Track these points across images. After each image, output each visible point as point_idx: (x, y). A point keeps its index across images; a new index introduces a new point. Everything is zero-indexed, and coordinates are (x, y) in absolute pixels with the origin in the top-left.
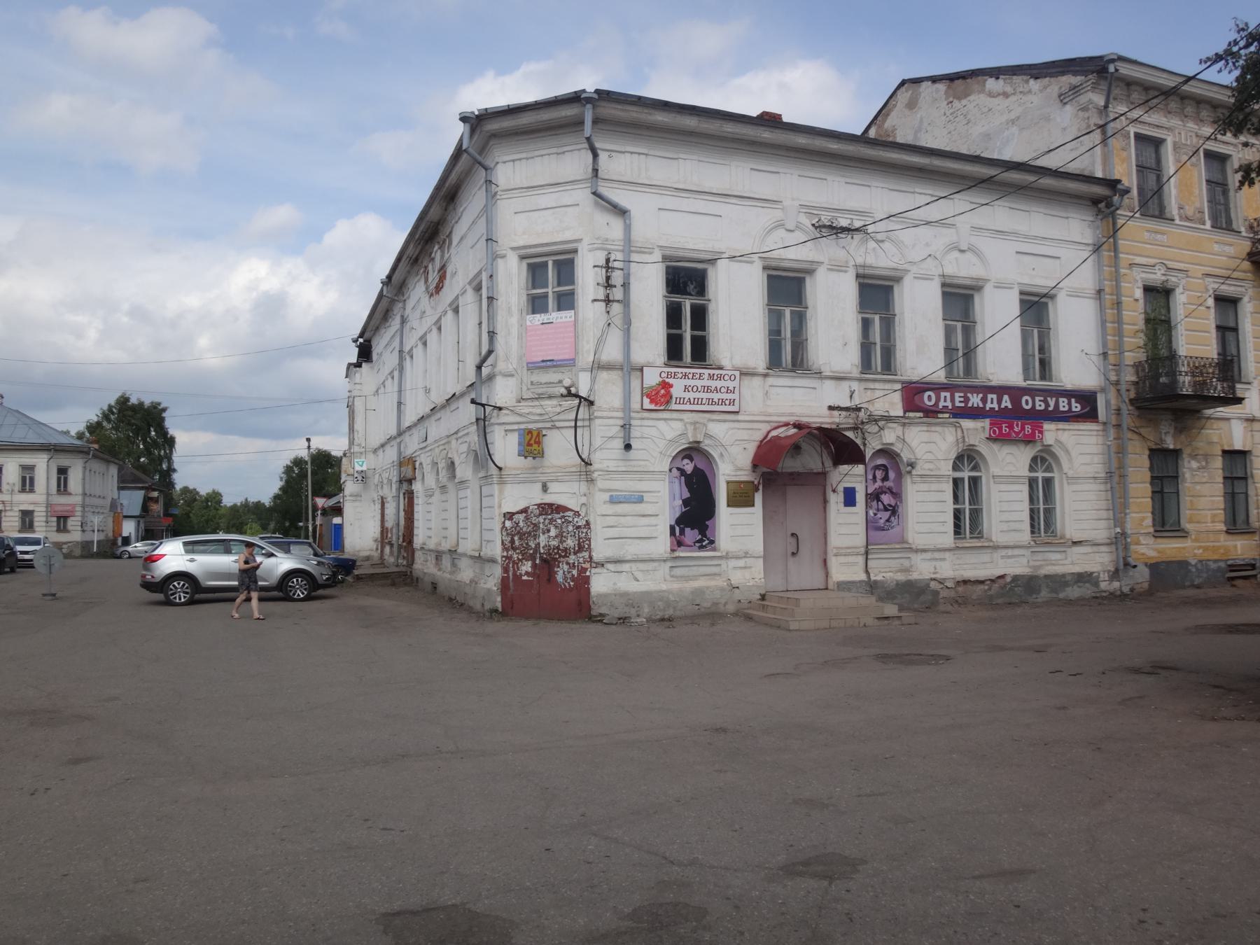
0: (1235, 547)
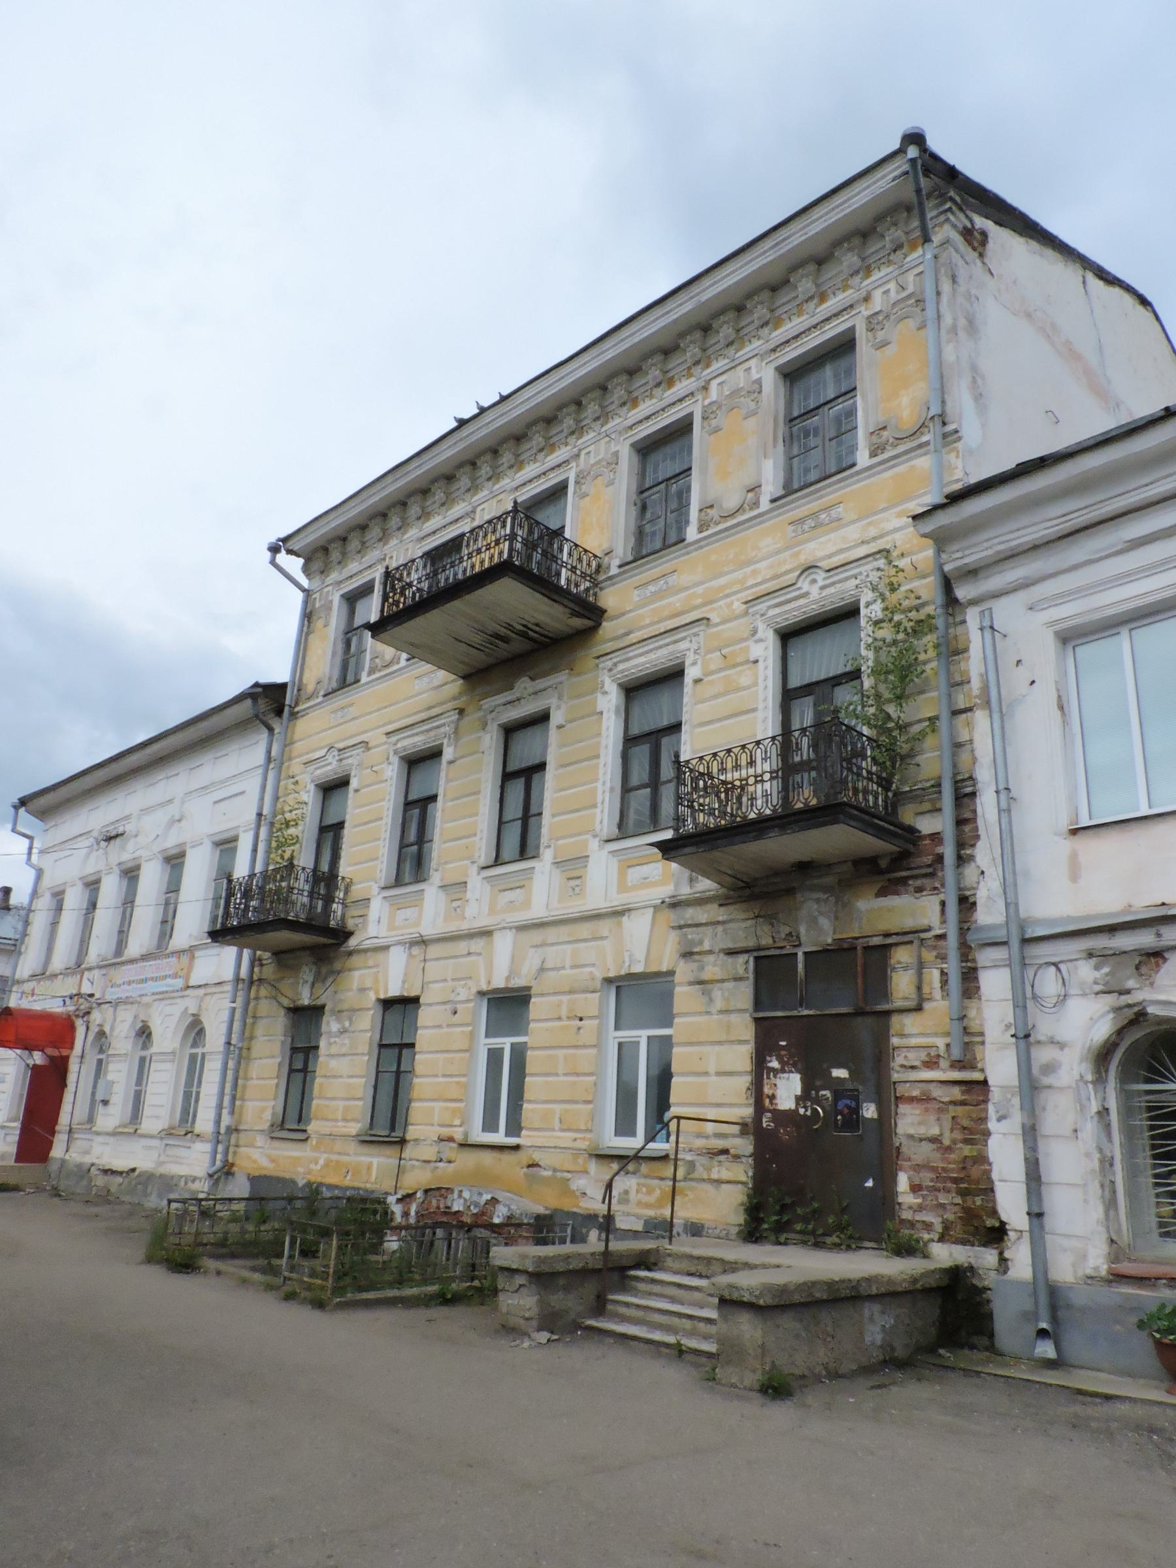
0: (369, 1167)
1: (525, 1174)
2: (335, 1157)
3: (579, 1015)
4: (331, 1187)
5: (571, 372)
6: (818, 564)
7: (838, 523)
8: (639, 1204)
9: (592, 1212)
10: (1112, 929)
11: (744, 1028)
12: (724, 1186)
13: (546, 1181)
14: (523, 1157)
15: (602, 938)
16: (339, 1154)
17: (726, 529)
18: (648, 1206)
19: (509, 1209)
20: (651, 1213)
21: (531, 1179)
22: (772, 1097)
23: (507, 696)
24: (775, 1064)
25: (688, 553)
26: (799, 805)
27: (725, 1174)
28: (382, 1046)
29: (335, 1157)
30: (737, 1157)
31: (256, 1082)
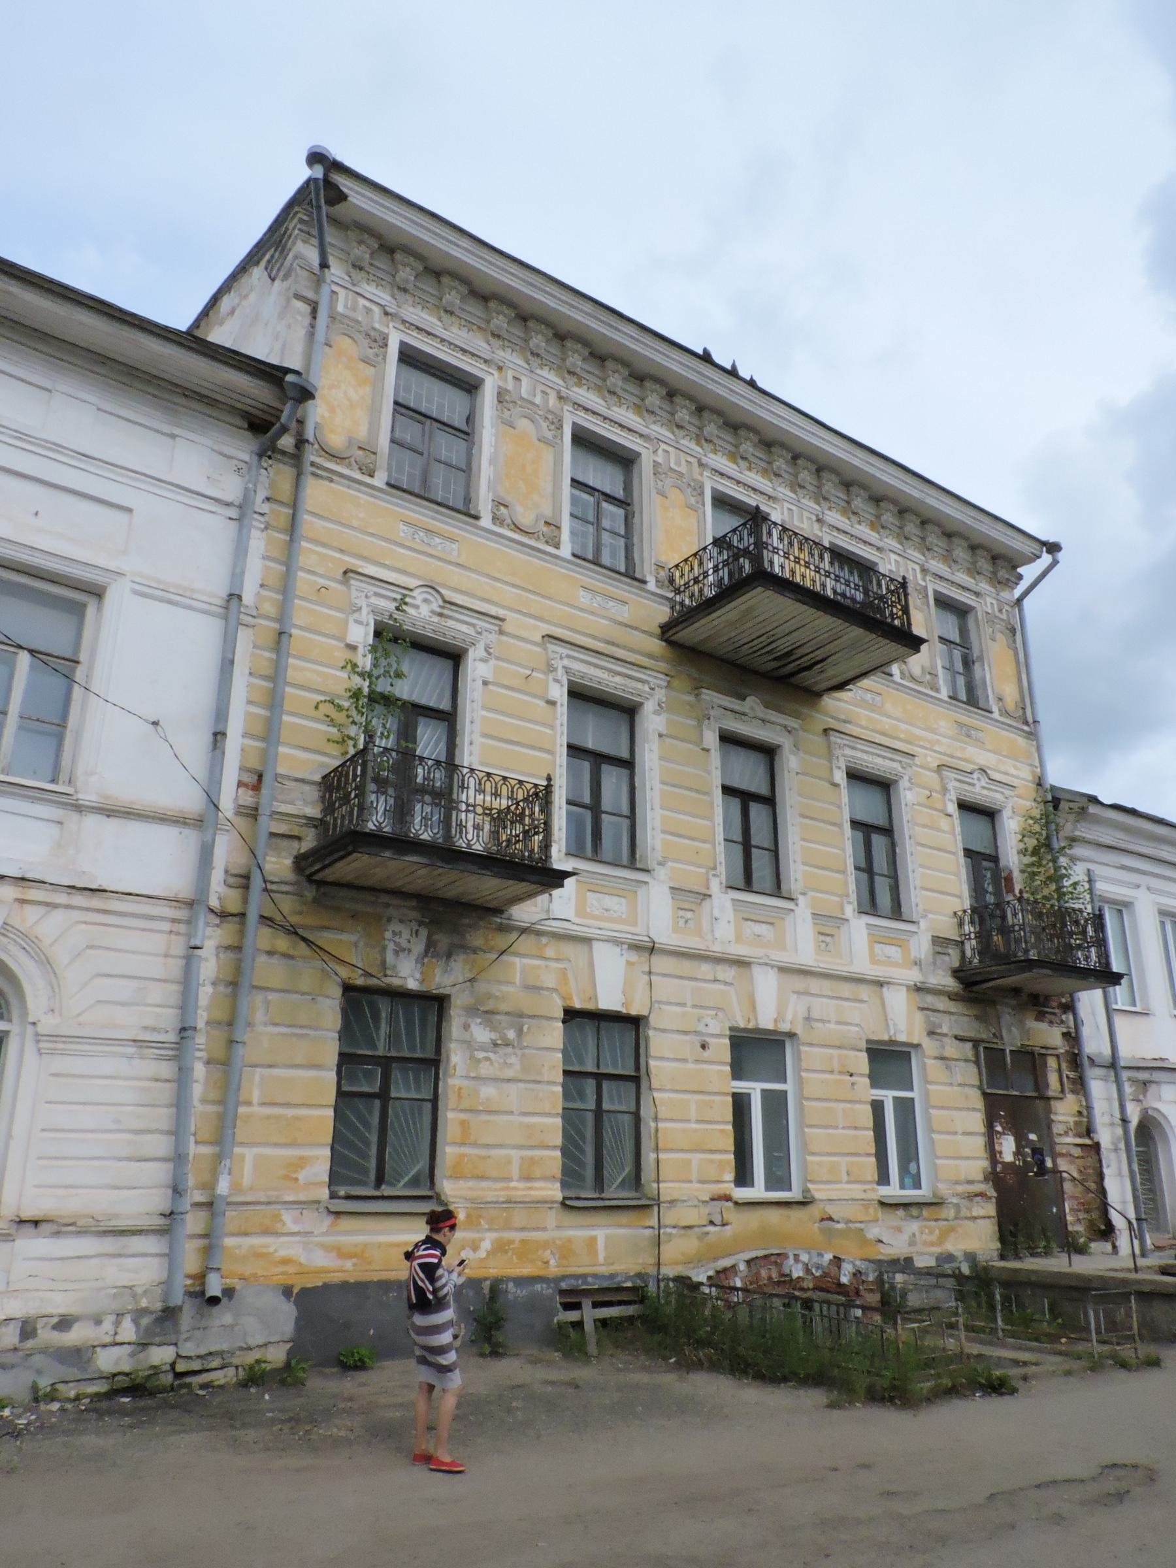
1: (820, 1229)
2: (517, 1236)
3: (851, 1071)
4: (520, 1281)
5: (790, 422)
6: (989, 772)
7: (980, 744)
8: (925, 1243)
9: (896, 1257)
10: (1138, 1068)
11: (978, 1101)
12: (978, 1221)
13: (841, 1233)
14: (815, 1211)
15: (861, 1001)
16: (523, 1229)
17: (919, 692)
18: (932, 1244)
19: (854, 1265)
20: (937, 1250)
21: (829, 1234)
22: (1001, 1153)
23: (735, 704)
24: (999, 1128)
25: (888, 686)
26: (371, 826)
27: (982, 1212)
28: (636, 1080)
29: (517, 1236)
30: (990, 1198)
31: (256, 1109)
